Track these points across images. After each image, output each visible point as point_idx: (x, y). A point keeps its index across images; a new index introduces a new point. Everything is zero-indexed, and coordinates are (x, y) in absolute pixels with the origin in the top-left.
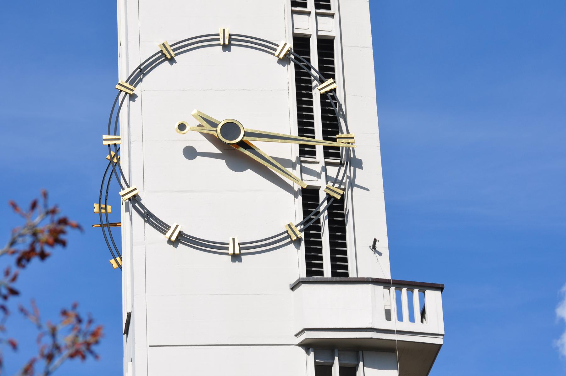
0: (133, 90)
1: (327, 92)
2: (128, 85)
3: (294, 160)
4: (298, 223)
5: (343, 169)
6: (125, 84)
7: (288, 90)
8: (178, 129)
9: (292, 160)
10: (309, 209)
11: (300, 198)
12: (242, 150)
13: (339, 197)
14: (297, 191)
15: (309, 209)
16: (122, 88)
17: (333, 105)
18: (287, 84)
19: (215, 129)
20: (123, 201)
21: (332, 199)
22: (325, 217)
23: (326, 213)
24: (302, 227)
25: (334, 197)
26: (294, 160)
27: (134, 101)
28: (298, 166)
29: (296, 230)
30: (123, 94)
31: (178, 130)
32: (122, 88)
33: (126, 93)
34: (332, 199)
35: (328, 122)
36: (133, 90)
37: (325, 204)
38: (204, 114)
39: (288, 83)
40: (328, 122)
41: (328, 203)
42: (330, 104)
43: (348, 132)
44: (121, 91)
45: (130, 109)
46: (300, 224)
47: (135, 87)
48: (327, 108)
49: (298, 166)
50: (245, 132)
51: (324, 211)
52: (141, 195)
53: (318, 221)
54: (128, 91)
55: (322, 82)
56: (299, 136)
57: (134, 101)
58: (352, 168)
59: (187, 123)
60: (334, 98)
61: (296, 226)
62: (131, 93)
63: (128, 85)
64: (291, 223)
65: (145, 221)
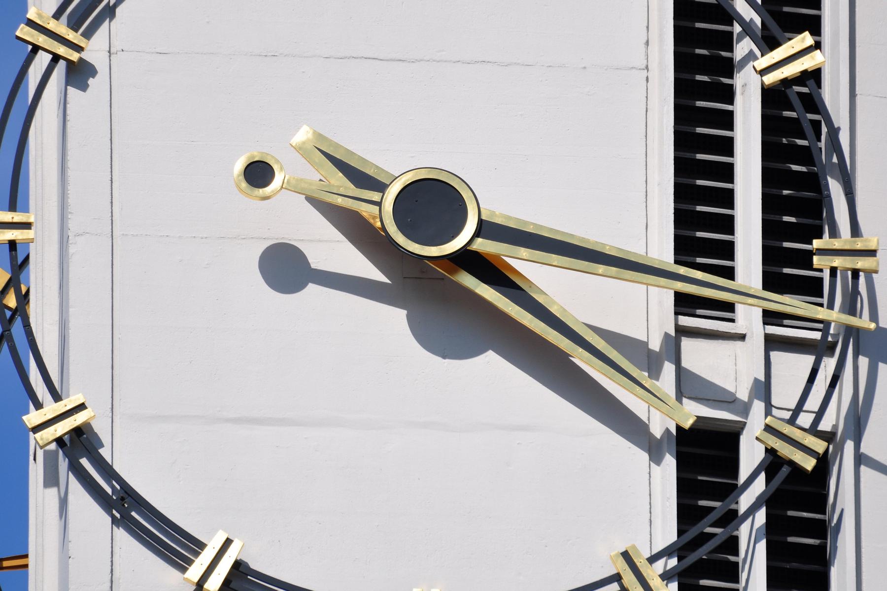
0: (78, 48)
1: (786, 83)
2: (61, 28)
3: (655, 345)
4: (659, 546)
5: (829, 365)
6: (52, 25)
7: (647, 68)
8: (242, 178)
9: (647, 344)
10: (702, 503)
11: (670, 463)
12: (468, 280)
13: (809, 464)
14: (658, 437)
15: (702, 503)
16: (41, 40)
17: (808, 129)
18: (643, 47)
19: (375, 196)
20: (38, 447)
21: (785, 470)
22: (757, 530)
23: (761, 517)
24: (673, 562)
25: (791, 463)
26: (655, 345)
27: (84, 87)
28: (669, 370)
29: (651, 573)
30: (42, 60)
31: (244, 184)
32: (41, 40)
33: (56, 58)
34: (785, 470)
35: (786, 192)
36: (78, 48)
37: (759, 485)
38: (337, 146)
39: (647, 43)
40: (786, 192)
41: (768, 481)
42: (795, 128)
43: (856, 231)
44: (36, 49)
45: (68, 118)
46: (666, 552)
47: (88, 35)
48: (784, 141)
49: (669, 370)
50: (481, 222)
51: (752, 510)
52: (101, 429)
53: (732, 545)
54: (62, 50)
55: (769, 43)
56: (677, 262)
57: (84, 87)
58: (863, 361)
59: (277, 161)
60: (813, 103)
61: (652, 560)
62: (74, 56)
63: (61, 28)
64: (634, 547)
65: (115, 521)
